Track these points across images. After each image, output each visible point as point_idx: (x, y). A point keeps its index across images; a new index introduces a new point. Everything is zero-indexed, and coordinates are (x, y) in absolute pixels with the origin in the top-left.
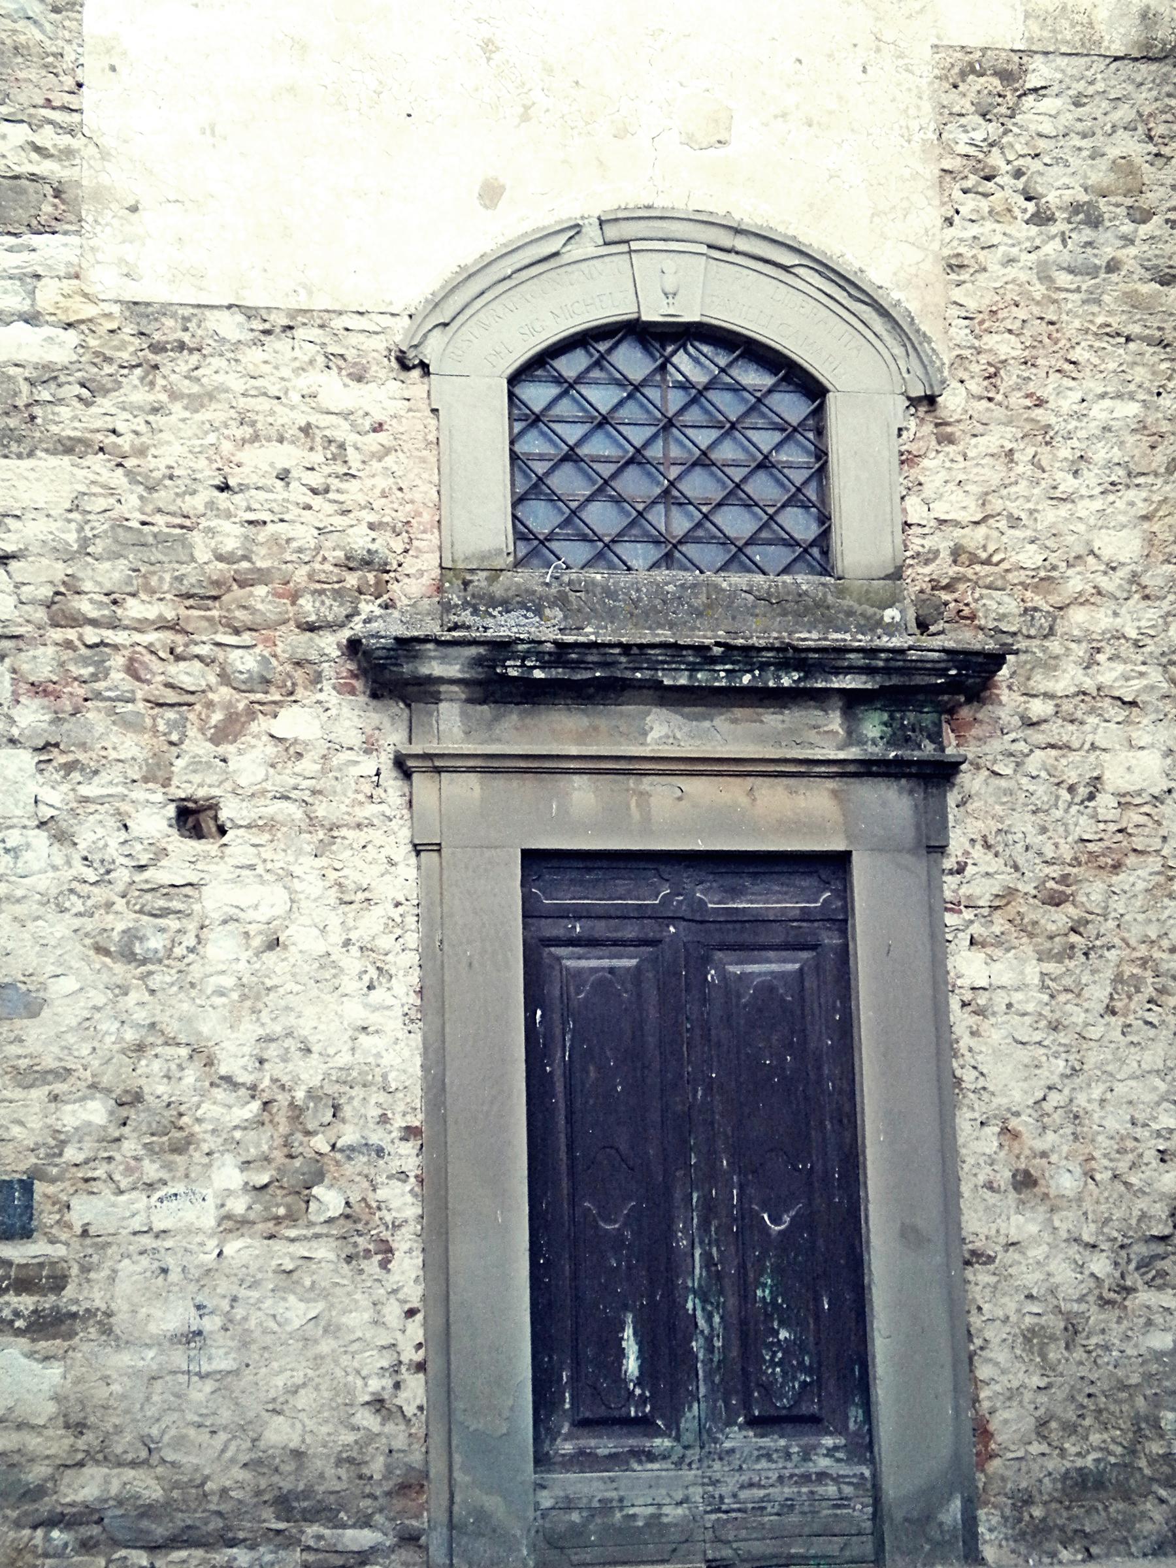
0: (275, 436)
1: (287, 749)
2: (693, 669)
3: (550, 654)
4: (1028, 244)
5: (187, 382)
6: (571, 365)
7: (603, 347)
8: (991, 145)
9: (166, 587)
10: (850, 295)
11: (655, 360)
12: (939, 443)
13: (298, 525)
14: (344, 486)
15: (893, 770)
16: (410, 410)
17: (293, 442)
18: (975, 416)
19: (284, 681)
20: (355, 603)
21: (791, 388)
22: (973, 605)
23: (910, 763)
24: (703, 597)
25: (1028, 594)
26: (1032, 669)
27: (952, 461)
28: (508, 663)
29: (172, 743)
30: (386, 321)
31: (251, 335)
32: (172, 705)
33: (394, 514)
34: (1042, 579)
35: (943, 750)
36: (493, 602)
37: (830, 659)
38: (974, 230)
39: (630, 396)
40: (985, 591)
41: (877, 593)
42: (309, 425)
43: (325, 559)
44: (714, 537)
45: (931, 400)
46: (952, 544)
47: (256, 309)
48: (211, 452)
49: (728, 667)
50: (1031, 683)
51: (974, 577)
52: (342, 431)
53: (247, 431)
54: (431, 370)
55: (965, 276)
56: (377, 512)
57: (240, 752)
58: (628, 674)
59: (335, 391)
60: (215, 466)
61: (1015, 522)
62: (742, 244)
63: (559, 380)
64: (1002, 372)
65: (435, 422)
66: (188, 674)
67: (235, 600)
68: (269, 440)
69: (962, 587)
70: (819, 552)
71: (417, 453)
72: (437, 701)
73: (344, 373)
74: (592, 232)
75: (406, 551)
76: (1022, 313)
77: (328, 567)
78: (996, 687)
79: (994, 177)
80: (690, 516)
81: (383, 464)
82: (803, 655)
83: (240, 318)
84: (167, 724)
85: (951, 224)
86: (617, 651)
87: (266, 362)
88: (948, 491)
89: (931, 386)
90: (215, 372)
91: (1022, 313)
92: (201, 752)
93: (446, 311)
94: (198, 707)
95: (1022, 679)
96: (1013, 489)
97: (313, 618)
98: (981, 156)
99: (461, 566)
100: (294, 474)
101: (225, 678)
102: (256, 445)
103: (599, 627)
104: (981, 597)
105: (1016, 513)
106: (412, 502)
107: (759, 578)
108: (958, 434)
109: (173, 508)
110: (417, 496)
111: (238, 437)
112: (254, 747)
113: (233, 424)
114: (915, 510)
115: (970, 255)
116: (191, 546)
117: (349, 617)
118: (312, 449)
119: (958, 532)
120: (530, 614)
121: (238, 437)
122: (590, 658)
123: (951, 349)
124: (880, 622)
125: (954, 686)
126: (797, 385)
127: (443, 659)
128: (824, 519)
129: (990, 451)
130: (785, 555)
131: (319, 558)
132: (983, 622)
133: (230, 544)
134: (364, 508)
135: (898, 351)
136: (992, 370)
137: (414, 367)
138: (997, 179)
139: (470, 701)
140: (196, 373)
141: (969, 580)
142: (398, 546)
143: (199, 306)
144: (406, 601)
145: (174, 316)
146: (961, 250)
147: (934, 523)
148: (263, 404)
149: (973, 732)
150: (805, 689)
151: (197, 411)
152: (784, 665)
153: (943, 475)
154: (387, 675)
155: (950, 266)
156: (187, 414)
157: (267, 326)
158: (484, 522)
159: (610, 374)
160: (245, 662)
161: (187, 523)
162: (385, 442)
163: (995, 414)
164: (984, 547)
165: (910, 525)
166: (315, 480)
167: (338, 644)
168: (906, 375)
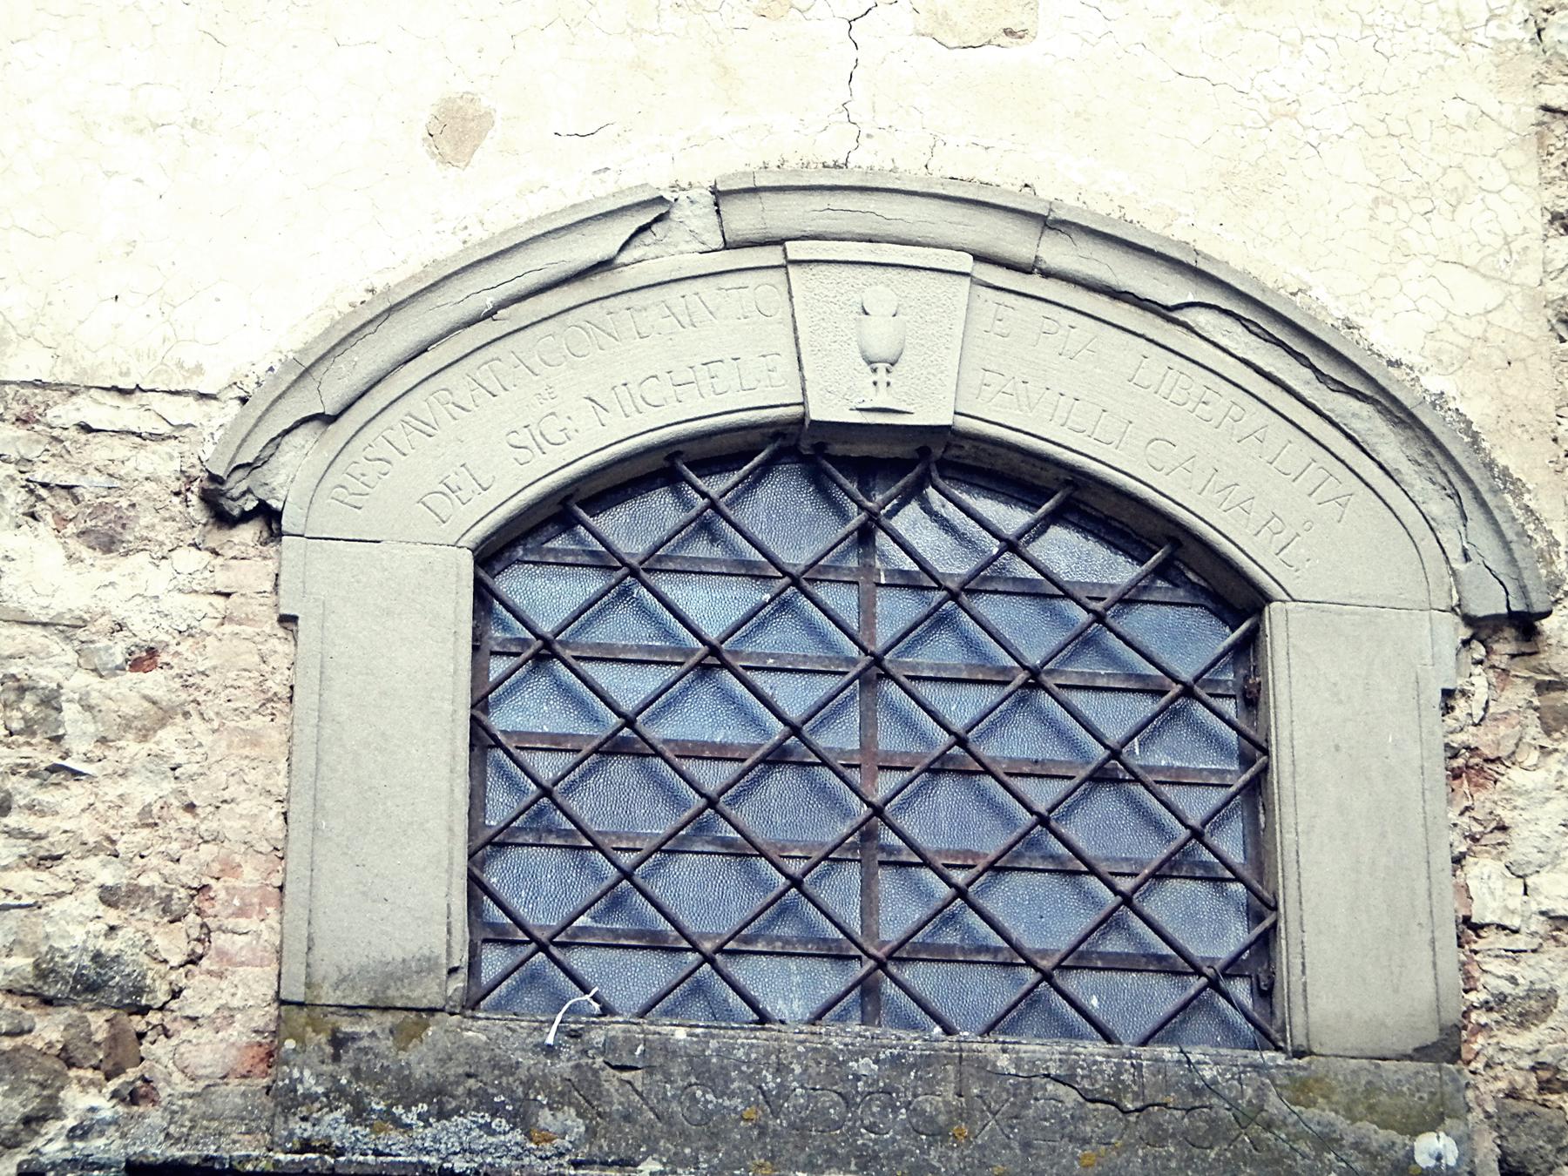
6: (630, 528)
7: (716, 485)
14: (47, 797)
16: (225, 619)
21: (1181, 594)
45: (1525, 625)
62: (1058, 252)
63: (604, 559)
74: (695, 218)
75: (194, 960)
81: (150, 746)
89: (1523, 590)
93: (325, 397)
99: (329, 996)
110: (230, 824)
114: (1490, 891)
117: (32, 1122)
120: (500, 1123)
128: (1263, 909)
134: (95, 850)
135: (1441, 508)
137: (246, 517)
142: (173, 943)
147: (1539, 925)
162: (158, 694)
165: (1478, 928)
168: (1459, 566)
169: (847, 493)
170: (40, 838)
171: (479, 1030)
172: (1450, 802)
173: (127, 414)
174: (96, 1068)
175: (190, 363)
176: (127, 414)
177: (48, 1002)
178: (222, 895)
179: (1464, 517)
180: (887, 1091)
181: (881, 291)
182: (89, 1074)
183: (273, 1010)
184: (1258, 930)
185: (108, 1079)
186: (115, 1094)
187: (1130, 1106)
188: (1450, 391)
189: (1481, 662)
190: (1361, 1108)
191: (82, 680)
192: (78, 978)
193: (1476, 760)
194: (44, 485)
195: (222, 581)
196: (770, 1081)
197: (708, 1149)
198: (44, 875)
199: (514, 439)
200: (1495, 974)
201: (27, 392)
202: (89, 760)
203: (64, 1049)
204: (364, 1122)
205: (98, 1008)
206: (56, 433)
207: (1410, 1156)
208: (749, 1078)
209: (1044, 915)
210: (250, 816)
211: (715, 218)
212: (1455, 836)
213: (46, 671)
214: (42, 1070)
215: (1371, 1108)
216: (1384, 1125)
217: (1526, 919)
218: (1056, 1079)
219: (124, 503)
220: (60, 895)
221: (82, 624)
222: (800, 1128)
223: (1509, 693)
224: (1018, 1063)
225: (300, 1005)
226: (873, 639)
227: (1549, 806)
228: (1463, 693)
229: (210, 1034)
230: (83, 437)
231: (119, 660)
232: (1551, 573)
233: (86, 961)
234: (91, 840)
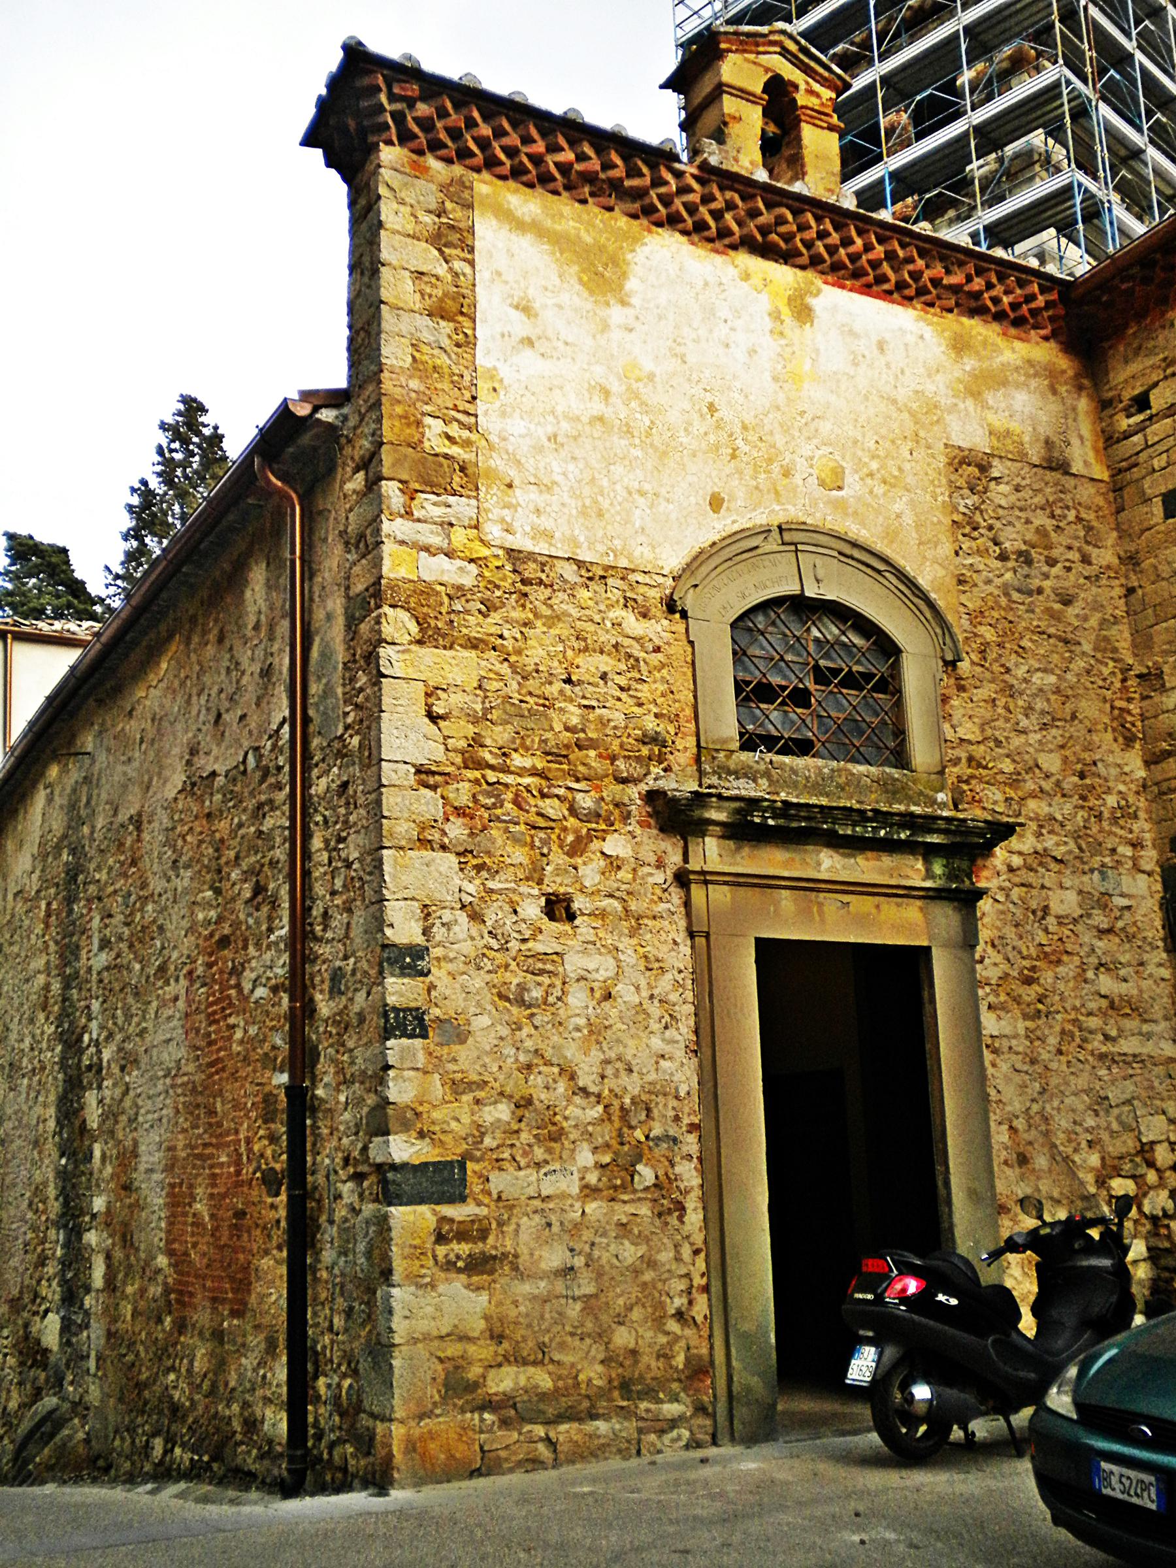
7: (286, 808)
14: (639, 687)
20: (648, 766)
29: (543, 855)
30: (661, 580)
36: (730, 773)
52: (636, 651)
57: (585, 864)
59: (633, 624)
62: (856, 553)
66: (552, 808)
69: (973, 782)
74: (775, 534)
76: (996, 614)
77: (631, 740)
91: (996, 614)
100: (610, 676)
109: (538, 692)
113: (573, 639)
116: (551, 720)
119: (972, 748)
127: (719, 809)
133: (575, 721)
135: (938, 631)
145: (535, 561)
148: (590, 627)
152: (903, 826)
153: (962, 711)
160: (586, 802)
166: (623, 682)
177: (644, 743)
181: (819, 561)
191: (643, 655)
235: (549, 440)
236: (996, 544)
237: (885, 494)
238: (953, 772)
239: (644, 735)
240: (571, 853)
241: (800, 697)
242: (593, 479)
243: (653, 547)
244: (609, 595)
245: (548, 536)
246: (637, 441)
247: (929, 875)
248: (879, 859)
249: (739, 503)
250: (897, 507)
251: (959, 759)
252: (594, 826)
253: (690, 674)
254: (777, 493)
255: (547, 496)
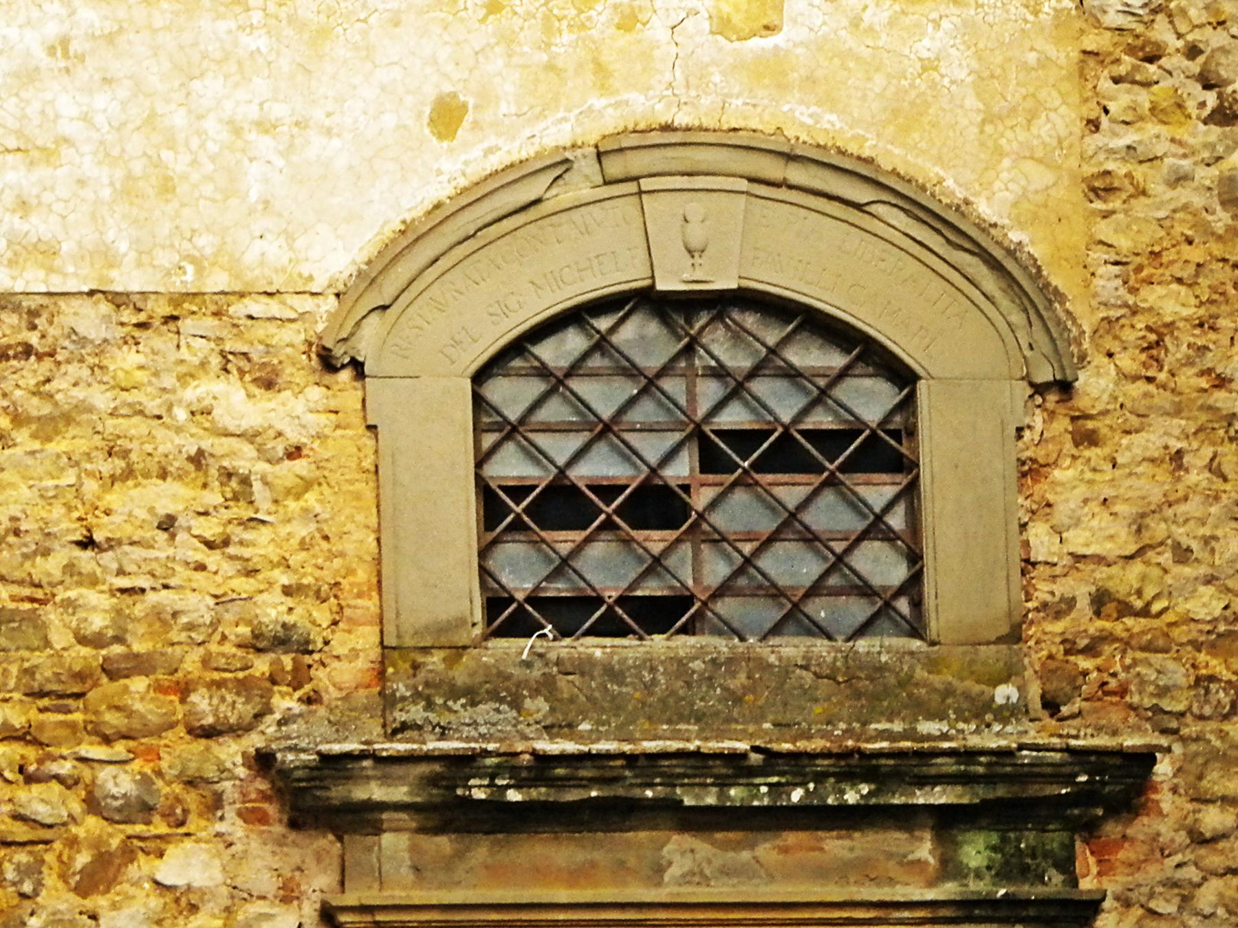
0: (155, 470)
1: (177, 901)
2: (723, 784)
3: (528, 768)
4: (1206, 154)
5: (35, 401)
6: (558, 351)
7: (603, 323)
8: (1155, 11)
9: (12, 683)
10: (948, 241)
11: (680, 339)
12: (1077, 445)
13: (188, 592)
14: (248, 536)
15: (1003, 913)
16: (338, 427)
17: (180, 477)
18: (1128, 405)
19: (172, 808)
20: (267, 695)
21: (871, 370)
22: (1122, 676)
23: (1027, 903)
24: (742, 677)
25: (1202, 657)
26: (1206, 763)
27: (1094, 470)
28: (472, 782)
29: (23, 896)
30: (306, 304)
31: (121, 332)
32: (23, 844)
33: (318, 573)
34: (1220, 635)
35: (1073, 882)
36: (454, 692)
37: (913, 766)
38: (1130, 137)
39: (644, 391)
40: (1140, 655)
41: (984, 664)
42: (200, 452)
43: (224, 638)
44: (760, 587)
45: (1065, 388)
46: (1093, 589)
47: (128, 295)
48: (70, 496)
49: (775, 779)
50: (1204, 783)
51: (1124, 635)
52: (245, 459)
53: (119, 464)
54: (367, 370)
55: (1115, 203)
56: (295, 571)
57: (114, 906)
58: (637, 792)
59: (236, 403)
60: (76, 515)
61: (1183, 555)
62: (796, 174)
63: (543, 372)
64: (1167, 339)
65: (370, 443)
66: (42, 802)
67: (105, 697)
68: (147, 475)
69: (1107, 649)
70: (903, 610)
71: (346, 487)
72: (378, 830)
73: (248, 378)
74: (587, 167)
75: (335, 623)
76: (1195, 254)
77: (229, 649)
78: (1156, 791)
79: (1159, 57)
80: (728, 557)
81: (302, 503)
82: (874, 762)
83: (105, 307)
84: (18, 868)
85: (1097, 128)
86: (619, 763)
87: (141, 367)
88: (1084, 519)
89: (1062, 368)
90: (69, 386)
91: (1195, 254)
92: (63, 907)
93: (379, 284)
94: (57, 846)
95: (1191, 778)
96: (1181, 509)
97: (210, 720)
98: (1140, 29)
99: (409, 642)
100: (181, 521)
101: (93, 804)
102: (130, 483)
103: (599, 723)
104: (1135, 662)
105: (1185, 541)
106: (342, 554)
107: (821, 646)
108: (1104, 431)
109: (18, 575)
110: (349, 546)
111: (106, 474)
112: (133, 897)
113: (100, 455)
114: (1041, 541)
115: (1123, 171)
116: (45, 626)
117: (258, 716)
118: (205, 486)
119: (1102, 573)
120: (504, 707)
121: (106, 474)
122: (583, 773)
123: (1093, 310)
124: (989, 705)
125: (1086, 796)
126: (875, 364)
127: (385, 780)
128: (914, 557)
129: (1148, 454)
130: (859, 610)
131: (217, 637)
132: (1136, 699)
133: (98, 622)
134: (279, 564)
135: (1017, 318)
136: (1153, 337)
137: (343, 366)
138: (1163, 61)
139: (421, 830)
140: (47, 387)
141: (1117, 640)
142: (323, 615)
143: (50, 294)
144: (334, 693)
145: (17, 308)
146: (1110, 166)
147: (1067, 561)
148: (137, 427)
149: (1121, 855)
150: (877, 807)
151: (49, 439)
152: (850, 777)
153: (1082, 491)
154: (309, 801)
155: (1094, 190)
156: (36, 445)
157: (142, 317)
158: (443, 578)
159: (617, 361)
160: (119, 784)
161: (39, 594)
162: (304, 473)
163: (1156, 400)
164: (1139, 593)
165: (1034, 564)
166: (210, 528)
167: (244, 754)
168: (1028, 353)
169: (675, 766)
170: (248, 560)
171: (489, 656)
172: (1020, 492)
173: (274, 308)
174: (288, 685)
175: (306, 274)
176: (274, 308)
177: (259, 651)
178: (347, 587)
179: (1030, 322)
180: (710, 678)
181: (696, 207)
182: (284, 689)
183: (379, 650)
184: (913, 571)
185: (295, 690)
186: (300, 700)
187: (841, 680)
188: (1026, 240)
189: (1039, 406)
190: (966, 673)
191: (262, 466)
192: (275, 637)
193: (1035, 466)
194: (231, 353)
195: (333, 404)
196: (647, 677)
197: (615, 715)
198: (252, 580)
199: (491, 310)
200: (1043, 591)
201: (216, 297)
202: (270, 514)
203: (271, 675)
204: (432, 710)
205: (286, 652)
206: (236, 321)
207: (993, 699)
208: (636, 676)
209: (793, 566)
210: (358, 542)
211: (597, 166)
212: (1021, 513)
213: (242, 463)
214: (261, 689)
215: (972, 673)
216: (978, 682)
217: (1061, 558)
218: (801, 667)
219: (275, 361)
220: (261, 592)
221: (257, 434)
222: (663, 701)
223: (1055, 425)
224: (780, 659)
225: (394, 648)
226: (695, 410)
227: (1076, 491)
228: (1029, 427)
229: (347, 664)
230: (250, 322)
231: (281, 455)
232: (1080, 351)
233: (279, 628)
234: (276, 559)
235: (51, 51)
236: (1207, 87)
237: (892, 23)
238: (1048, 634)
239: (257, 636)
240: (82, 890)
241: (656, 504)
242: (153, 115)
243: (290, 238)
244: (184, 353)
245: (46, 252)
246: (257, 17)
247: (949, 868)
248: (850, 837)
249: (504, 108)
250: (926, 46)
251: (1071, 603)
252: (139, 828)
253: (369, 495)
254: (600, 69)
255: (43, 172)
